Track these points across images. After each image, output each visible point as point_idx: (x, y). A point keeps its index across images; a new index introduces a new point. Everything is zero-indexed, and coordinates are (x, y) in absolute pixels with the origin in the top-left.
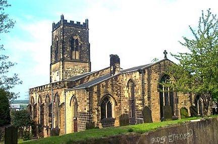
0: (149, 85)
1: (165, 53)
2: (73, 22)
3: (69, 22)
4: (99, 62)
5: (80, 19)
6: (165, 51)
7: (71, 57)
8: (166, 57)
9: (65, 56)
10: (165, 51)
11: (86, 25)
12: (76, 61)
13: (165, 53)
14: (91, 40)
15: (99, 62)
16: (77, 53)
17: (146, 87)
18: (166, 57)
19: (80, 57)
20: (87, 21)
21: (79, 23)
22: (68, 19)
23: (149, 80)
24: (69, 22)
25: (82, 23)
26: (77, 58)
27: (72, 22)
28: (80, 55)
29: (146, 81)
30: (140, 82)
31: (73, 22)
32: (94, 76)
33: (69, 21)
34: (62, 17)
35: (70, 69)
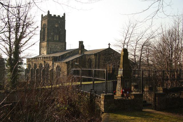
0: (99, 62)
1: (109, 44)
2: (56, 15)
3: (61, 17)
4: (72, 44)
5: (79, 42)
6: (109, 43)
7: (54, 39)
8: (109, 47)
9: (50, 38)
10: (109, 43)
11: (64, 17)
12: (56, 41)
13: (109, 44)
14: (67, 28)
15: (72, 44)
16: (58, 37)
17: (97, 63)
18: (109, 47)
19: (59, 39)
20: (64, 14)
21: (59, 16)
22: (52, 13)
23: (99, 59)
24: (61, 17)
25: (61, 17)
26: (57, 39)
27: (55, 16)
28: (59, 38)
29: (97, 60)
30: (94, 60)
31: (56, 15)
32: (69, 54)
33: (53, 15)
34: (49, 12)
35: (53, 47)
